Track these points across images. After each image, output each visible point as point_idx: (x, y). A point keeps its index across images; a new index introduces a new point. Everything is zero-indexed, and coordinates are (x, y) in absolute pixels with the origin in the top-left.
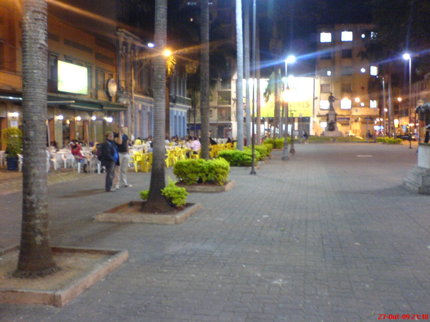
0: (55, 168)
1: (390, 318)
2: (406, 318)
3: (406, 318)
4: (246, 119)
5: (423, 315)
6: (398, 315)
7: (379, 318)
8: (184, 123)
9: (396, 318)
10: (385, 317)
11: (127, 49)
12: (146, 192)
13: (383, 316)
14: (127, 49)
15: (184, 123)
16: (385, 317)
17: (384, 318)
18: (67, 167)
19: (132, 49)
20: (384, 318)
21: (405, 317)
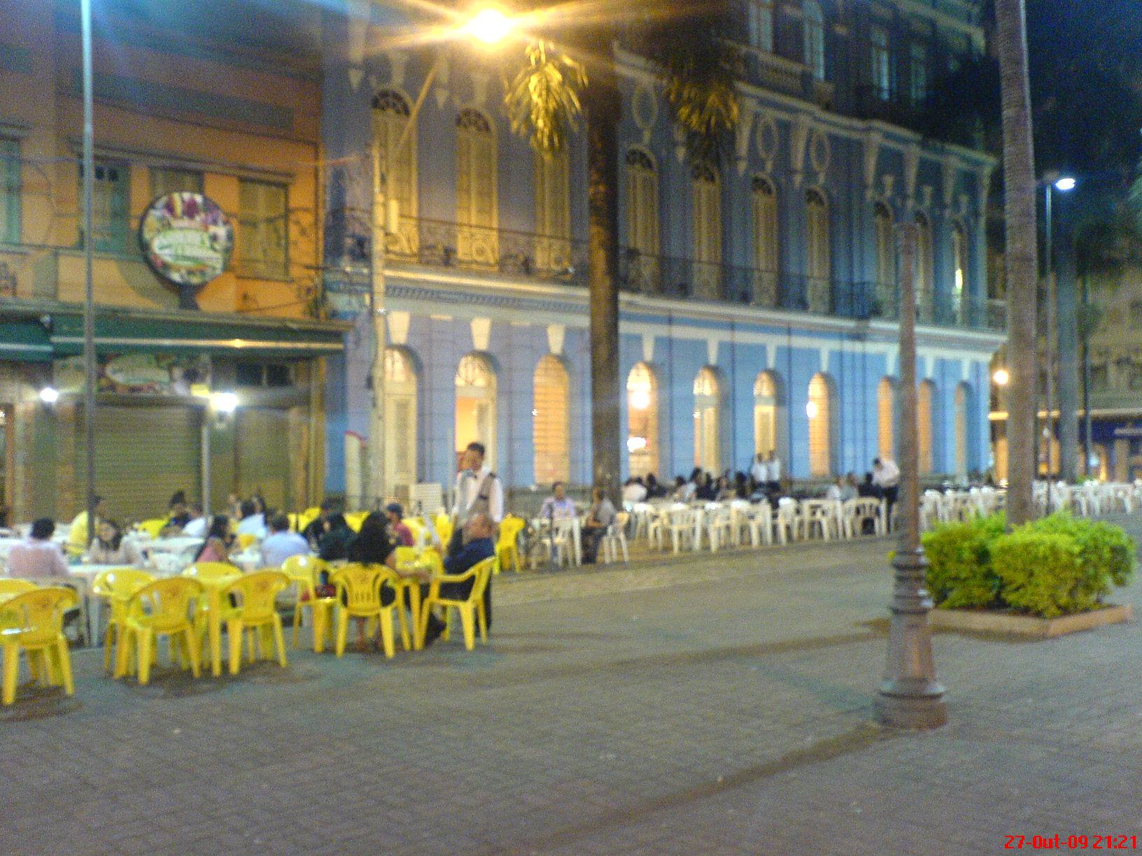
0: (714, 547)
1: (1035, 846)
2: (1079, 845)
3: (1079, 845)
4: (424, 505)
5: (1109, 838)
6: (1057, 839)
7: (1007, 846)
8: (702, 443)
9: (1051, 847)
10: (1021, 842)
11: (900, 186)
12: (43, 684)
13: (1017, 841)
14: (900, 186)
15: (702, 443)
16: (1021, 842)
17: (1020, 847)
18: (681, 549)
19: (922, 179)
20: (1020, 847)
21: (1077, 841)
